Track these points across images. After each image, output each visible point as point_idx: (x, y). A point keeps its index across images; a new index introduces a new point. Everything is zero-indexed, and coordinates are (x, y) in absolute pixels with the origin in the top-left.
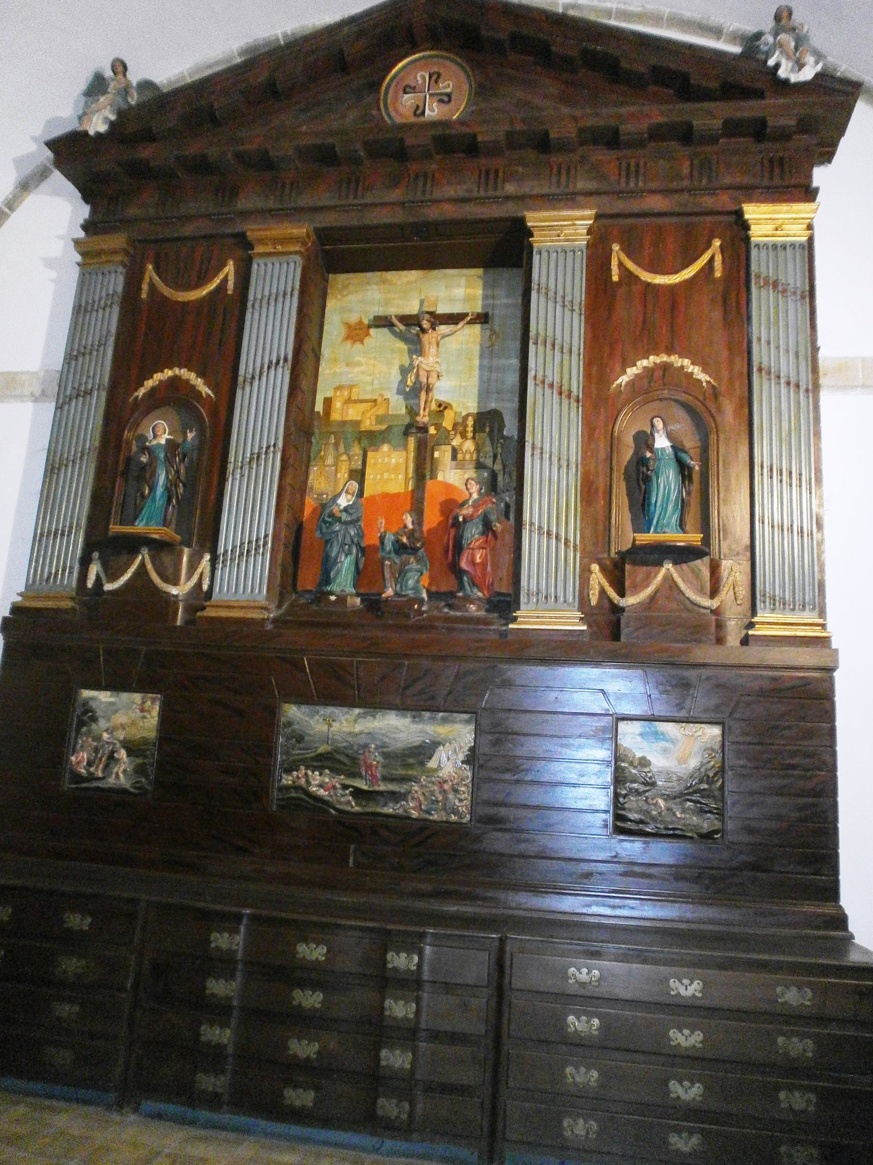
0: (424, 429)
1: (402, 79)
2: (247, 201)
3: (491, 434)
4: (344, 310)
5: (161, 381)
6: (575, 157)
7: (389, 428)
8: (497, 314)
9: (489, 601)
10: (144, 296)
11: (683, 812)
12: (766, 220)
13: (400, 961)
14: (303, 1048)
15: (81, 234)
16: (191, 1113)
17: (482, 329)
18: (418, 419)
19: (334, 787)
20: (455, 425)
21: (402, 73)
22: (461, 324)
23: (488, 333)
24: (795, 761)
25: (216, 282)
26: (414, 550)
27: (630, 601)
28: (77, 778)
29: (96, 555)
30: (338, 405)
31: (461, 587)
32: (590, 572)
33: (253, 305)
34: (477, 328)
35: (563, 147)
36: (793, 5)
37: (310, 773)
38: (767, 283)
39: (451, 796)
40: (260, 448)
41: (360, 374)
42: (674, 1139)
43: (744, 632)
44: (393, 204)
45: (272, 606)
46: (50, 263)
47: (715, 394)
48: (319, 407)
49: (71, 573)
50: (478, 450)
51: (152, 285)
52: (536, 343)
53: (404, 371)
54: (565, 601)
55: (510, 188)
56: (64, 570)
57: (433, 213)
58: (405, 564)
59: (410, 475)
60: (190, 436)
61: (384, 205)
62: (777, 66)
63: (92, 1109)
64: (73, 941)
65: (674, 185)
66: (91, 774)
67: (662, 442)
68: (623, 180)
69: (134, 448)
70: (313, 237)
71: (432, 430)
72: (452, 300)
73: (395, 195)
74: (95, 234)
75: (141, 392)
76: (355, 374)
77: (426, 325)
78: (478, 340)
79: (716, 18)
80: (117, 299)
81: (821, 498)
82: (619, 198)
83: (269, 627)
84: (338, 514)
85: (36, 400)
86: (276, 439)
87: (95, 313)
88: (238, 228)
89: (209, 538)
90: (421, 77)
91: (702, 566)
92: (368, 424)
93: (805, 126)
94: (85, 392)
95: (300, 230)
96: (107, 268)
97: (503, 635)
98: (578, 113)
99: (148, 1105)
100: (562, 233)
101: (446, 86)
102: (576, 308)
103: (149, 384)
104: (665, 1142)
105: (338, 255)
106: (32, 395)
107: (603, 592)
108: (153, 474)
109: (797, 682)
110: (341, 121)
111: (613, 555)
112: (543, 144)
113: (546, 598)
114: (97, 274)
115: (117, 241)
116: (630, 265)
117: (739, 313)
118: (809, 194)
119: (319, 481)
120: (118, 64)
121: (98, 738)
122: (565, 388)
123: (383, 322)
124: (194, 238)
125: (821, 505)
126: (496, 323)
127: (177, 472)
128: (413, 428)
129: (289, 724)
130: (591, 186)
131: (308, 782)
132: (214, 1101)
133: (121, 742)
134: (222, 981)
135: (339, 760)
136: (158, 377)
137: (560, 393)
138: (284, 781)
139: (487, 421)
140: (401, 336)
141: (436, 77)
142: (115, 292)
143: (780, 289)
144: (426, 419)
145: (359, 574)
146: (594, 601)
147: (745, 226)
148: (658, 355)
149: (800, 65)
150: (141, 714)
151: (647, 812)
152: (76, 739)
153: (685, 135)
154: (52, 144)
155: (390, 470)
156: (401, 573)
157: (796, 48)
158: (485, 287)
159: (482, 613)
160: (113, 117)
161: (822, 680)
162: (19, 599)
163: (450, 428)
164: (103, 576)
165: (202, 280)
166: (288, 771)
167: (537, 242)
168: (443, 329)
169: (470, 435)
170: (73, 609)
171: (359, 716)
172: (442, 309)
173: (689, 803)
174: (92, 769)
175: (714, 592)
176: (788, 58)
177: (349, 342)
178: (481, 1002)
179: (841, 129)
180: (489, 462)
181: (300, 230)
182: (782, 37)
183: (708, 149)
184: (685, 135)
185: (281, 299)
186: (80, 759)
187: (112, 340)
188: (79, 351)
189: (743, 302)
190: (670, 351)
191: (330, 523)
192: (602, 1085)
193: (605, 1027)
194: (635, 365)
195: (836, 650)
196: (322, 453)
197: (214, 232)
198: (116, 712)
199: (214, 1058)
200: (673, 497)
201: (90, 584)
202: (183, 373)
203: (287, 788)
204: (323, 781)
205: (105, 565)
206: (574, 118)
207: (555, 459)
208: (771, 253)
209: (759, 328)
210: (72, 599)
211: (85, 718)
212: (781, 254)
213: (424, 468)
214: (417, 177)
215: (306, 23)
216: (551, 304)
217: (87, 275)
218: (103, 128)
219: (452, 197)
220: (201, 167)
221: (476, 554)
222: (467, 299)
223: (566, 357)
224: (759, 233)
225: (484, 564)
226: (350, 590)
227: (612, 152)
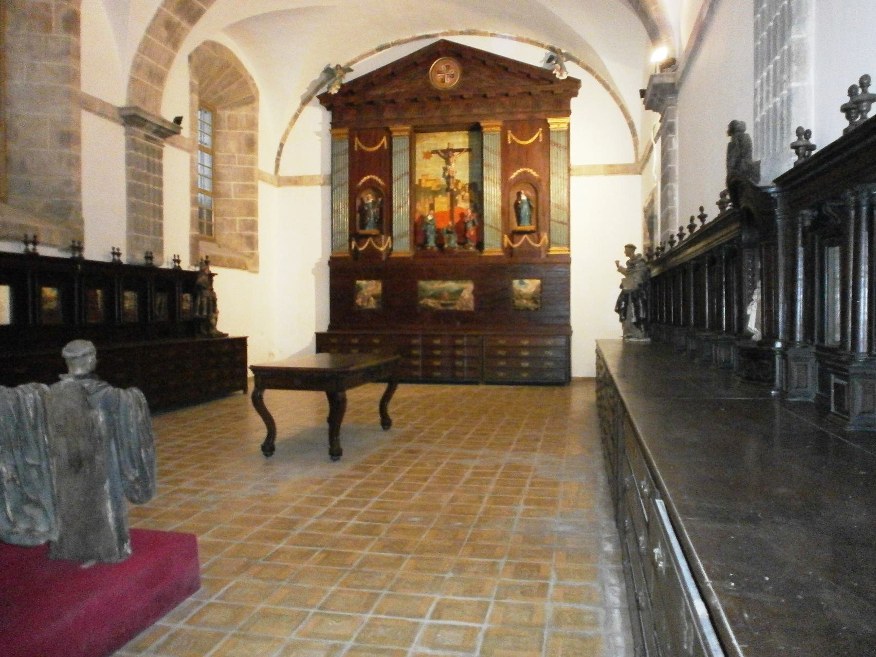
2: (388, 114)
13: (459, 342)
14: (437, 363)
27: (515, 246)
28: (359, 307)
30: (423, 181)
41: (430, 170)
46: (318, 134)
48: (417, 183)
51: (359, 147)
67: (524, 197)
75: (360, 184)
76: (427, 171)
89: (390, 231)
91: (535, 235)
92: (434, 188)
97: (480, 257)
116: (514, 138)
130: (502, 111)
135: (437, 296)
136: (365, 178)
140: (443, 157)
147: (548, 125)
155: (442, 203)
156: (449, 239)
165: (375, 144)
186: (359, 301)
190: (526, 166)
205: (357, 241)
209: (553, 160)
213: (453, 202)
218: (336, 92)
219: (455, 112)
222: (464, 143)
224: (552, 127)
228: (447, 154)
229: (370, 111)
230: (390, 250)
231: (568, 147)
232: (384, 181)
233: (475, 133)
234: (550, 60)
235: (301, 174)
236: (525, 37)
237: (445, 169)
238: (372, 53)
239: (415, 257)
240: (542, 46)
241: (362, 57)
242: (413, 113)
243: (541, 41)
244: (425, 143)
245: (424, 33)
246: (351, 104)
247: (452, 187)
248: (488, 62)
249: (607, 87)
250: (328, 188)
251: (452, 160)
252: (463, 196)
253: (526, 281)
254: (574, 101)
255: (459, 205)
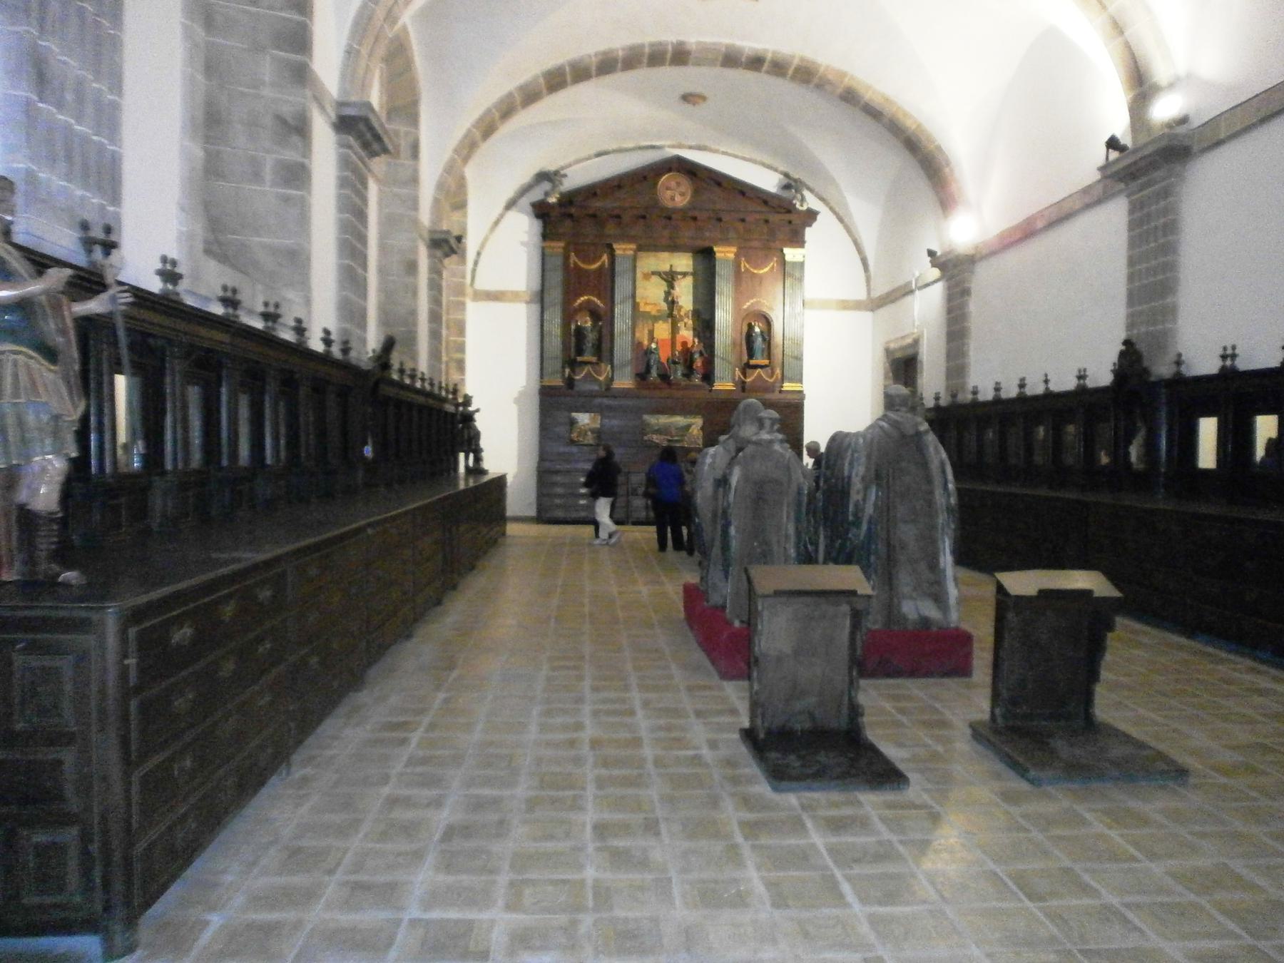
2: (611, 229)
12: (791, 254)
27: (748, 380)
41: (651, 293)
46: (523, 244)
67: (757, 330)
92: (654, 313)
119: (637, 335)
147: (784, 255)
155: (662, 330)
156: (676, 371)
165: (594, 261)
213: (674, 330)
219: (687, 234)
228: (670, 278)
229: (584, 226)
234: (787, 187)
235: (502, 288)
236: (759, 159)
237: (668, 294)
238: (589, 158)
240: (776, 170)
241: (578, 161)
242: (637, 230)
243: (776, 164)
245: (649, 143)
246: (570, 216)
247: (675, 312)
248: (725, 184)
249: (841, 220)
250: (536, 308)
251: (676, 284)
254: (808, 231)
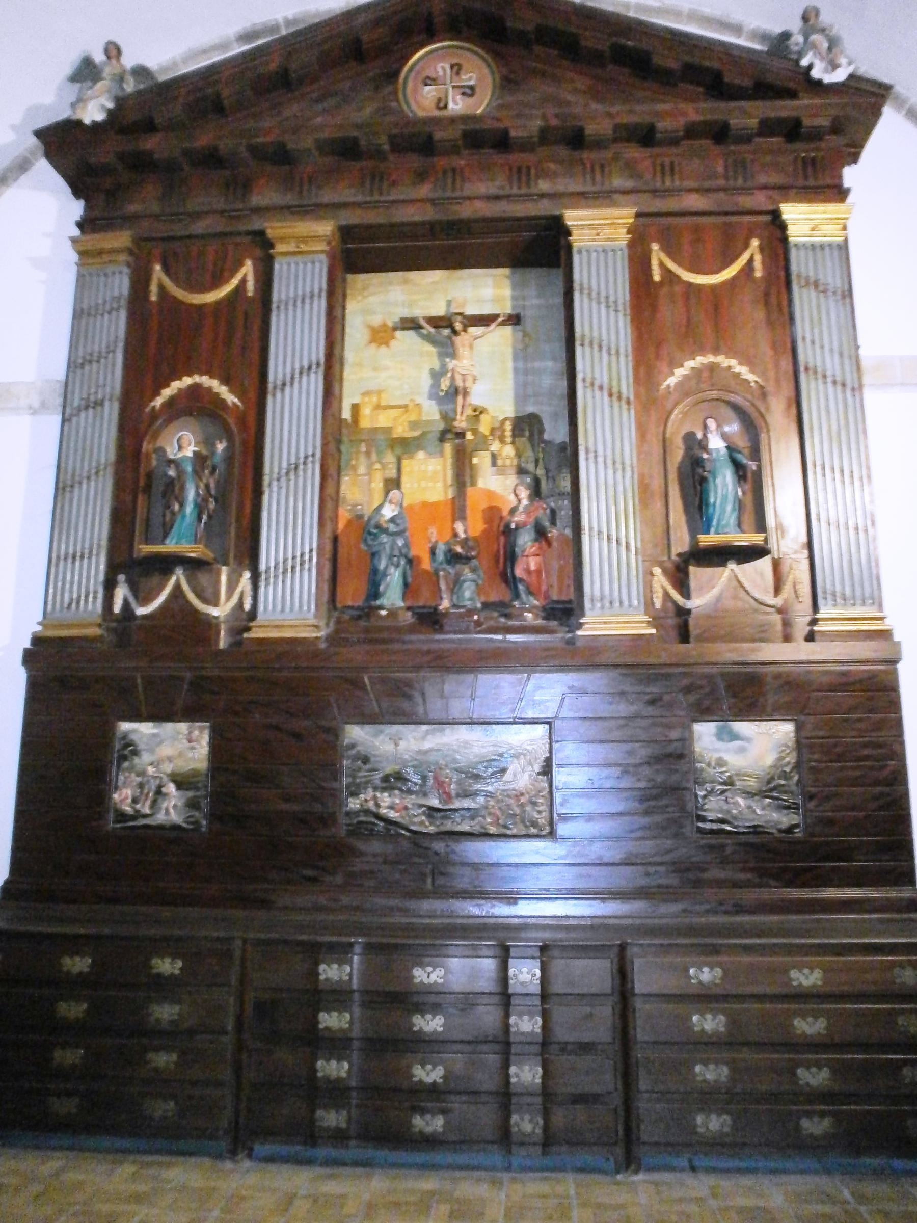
0: (461, 435)
1: (423, 69)
2: (265, 195)
3: (531, 438)
4: (366, 312)
5: (180, 390)
6: (608, 154)
7: (424, 434)
8: (529, 315)
9: (544, 609)
10: (154, 298)
11: (763, 809)
12: (802, 219)
15: (76, 232)
16: (310, 1152)
17: (514, 331)
18: (456, 424)
19: (406, 808)
20: (493, 430)
21: (421, 64)
22: (493, 326)
23: (520, 334)
24: (866, 752)
25: (235, 282)
26: (466, 559)
28: (122, 816)
29: (121, 578)
30: (366, 411)
31: (517, 596)
32: (652, 574)
33: (278, 307)
34: (508, 330)
35: (599, 144)
36: (819, 5)
37: (378, 795)
38: (807, 284)
39: (528, 808)
40: (298, 458)
41: (389, 378)
42: (805, 1123)
43: (808, 628)
44: (422, 201)
45: (322, 623)
47: (764, 395)
48: (346, 414)
49: (95, 598)
50: (519, 455)
51: (161, 287)
52: (582, 345)
53: (436, 376)
54: (630, 606)
55: (544, 186)
56: (87, 596)
57: (466, 211)
58: (458, 575)
59: (449, 482)
60: (220, 447)
61: (412, 202)
62: (810, 67)
63: (193, 1160)
64: (164, 987)
65: (707, 184)
66: (137, 811)
67: (716, 443)
68: (658, 179)
69: (154, 463)
70: (337, 236)
71: (469, 436)
72: (479, 301)
73: (425, 190)
74: (94, 230)
75: (158, 402)
77: (458, 326)
78: (510, 342)
79: (736, 16)
80: (123, 302)
81: (871, 495)
82: (655, 196)
83: (323, 646)
84: (385, 526)
85: (34, 412)
86: (314, 447)
87: (99, 317)
88: (256, 224)
89: (249, 554)
90: (442, 68)
92: (401, 431)
93: (836, 128)
94: (96, 403)
95: (325, 228)
96: (110, 269)
98: (614, 110)
99: (260, 1149)
100: (599, 232)
101: (469, 78)
102: (620, 308)
103: (167, 393)
104: (797, 1128)
105: (362, 253)
106: (30, 408)
107: (666, 595)
108: (183, 488)
109: (866, 675)
110: (358, 113)
111: (674, 557)
112: (576, 139)
113: (611, 603)
114: (98, 275)
115: (122, 239)
117: (781, 310)
118: (839, 193)
120: (111, 47)
121: (142, 773)
122: (615, 390)
123: (411, 324)
124: (202, 237)
125: (872, 502)
126: (528, 324)
127: (207, 486)
128: (449, 433)
129: (353, 746)
130: (629, 184)
131: (377, 805)
132: (339, 1137)
133: (168, 775)
134: (335, 1014)
136: (176, 386)
137: (611, 395)
138: (351, 805)
139: (526, 426)
140: (429, 339)
141: (457, 69)
142: (121, 295)
143: (821, 288)
144: (464, 425)
145: (407, 588)
146: (658, 604)
148: (704, 356)
149: (834, 66)
150: (188, 745)
151: (728, 812)
152: (117, 775)
153: (720, 133)
154: (39, 134)
155: (428, 478)
156: (456, 584)
157: (830, 49)
158: (514, 287)
159: (540, 622)
160: (110, 105)
161: (885, 672)
162: (39, 628)
163: (487, 433)
164: (132, 600)
165: (217, 281)
166: (354, 794)
167: (576, 241)
168: (473, 330)
169: (509, 439)
170: (102, 636)
171: (427, 733)
172: (471, 310)
173: (768, 800)
174: (138, 806)
175: (777, 590)
176: (822, 59)
177: (373, 345)
178: (606, 1012)
179: (868, 129)
180: (531, 467)
181: (325, 228)
182: (815, 37)
183: (744, 147)
184: (720, 133)
185: (307, 301)
186: (123, 797)
187: (121, 345)
188: (84, 358)
189: (785, 303)
190: (716, 351)
191: (375, 535)
192: (732, 1079)
193: (733, 1022)
194: (682, 366)
195: (899, 643)
196: (353, 462)
197: (228, 229)
198: (161, 742)
199: (336, 1093)
200: (731, 498)
201: (117, 608)
202: (205, 381)
203: (357, 813)
204: (393, 803)
205: (133, 586)
206: (610, 115)
207: (609, 462)
208: (810, 253)
209: (803, 328)
210: (100, 626)
211: (126, 752)
212: (819, 252)
214: (445, 172)
215: (308, 8)
216: (594, 304)
217: (87, 278)
218: (100, 117)
219: (483, 194)
220: (211, 159)
221: (529, 559)
222: (497, 300)
223: (614, 358)
225: (538, 572)
226: (401, 604)
227: (649, 150)
230: (246, 618)
231: (848, 294)
232: (242, 395)
233: (533, 275)
239: (334, 639)
244: (373, 300)
252: (494, 457)
253: (741, 727)
255: (481, 483)
